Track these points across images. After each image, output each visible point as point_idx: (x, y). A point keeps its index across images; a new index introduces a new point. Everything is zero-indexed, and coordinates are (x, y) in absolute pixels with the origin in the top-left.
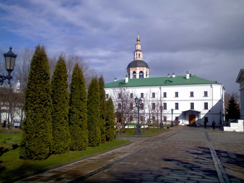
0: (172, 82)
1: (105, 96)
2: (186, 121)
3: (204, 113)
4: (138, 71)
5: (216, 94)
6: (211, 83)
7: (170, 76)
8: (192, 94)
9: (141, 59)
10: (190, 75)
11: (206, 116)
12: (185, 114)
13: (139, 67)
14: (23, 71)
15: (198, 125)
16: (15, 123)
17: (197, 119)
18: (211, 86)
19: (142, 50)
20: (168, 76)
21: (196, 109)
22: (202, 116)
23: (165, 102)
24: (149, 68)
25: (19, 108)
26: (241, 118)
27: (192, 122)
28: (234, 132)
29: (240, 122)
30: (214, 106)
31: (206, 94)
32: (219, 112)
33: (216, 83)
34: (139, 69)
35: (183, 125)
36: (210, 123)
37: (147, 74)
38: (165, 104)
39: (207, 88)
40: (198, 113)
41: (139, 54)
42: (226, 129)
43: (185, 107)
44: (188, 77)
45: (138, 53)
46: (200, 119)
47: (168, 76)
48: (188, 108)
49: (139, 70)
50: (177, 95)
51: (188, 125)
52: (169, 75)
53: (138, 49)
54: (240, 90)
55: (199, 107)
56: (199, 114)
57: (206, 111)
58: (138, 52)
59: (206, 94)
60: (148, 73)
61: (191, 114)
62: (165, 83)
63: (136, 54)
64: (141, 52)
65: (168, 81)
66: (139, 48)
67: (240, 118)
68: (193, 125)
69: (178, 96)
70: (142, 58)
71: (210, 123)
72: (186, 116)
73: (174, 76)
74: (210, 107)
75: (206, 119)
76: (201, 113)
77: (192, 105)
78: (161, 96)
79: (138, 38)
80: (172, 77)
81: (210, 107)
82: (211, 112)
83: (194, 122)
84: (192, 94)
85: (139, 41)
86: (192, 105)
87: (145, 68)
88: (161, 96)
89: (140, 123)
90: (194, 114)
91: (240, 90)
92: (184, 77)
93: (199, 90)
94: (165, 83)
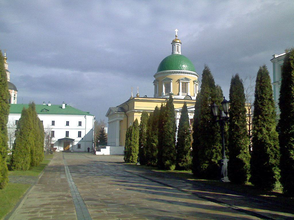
0: (48, 111)
2: (61, 148)
3: (77, 140)
5: (88, 124)
6: (85, 114)
7: (45, 104)
8: (68, 123)
10: (66, 105)
11: (79, 144)
12: (60, 141)
15: (72, 151)
17: (71, 146)
18: (85, 117)
19: (8, 70)
20: (44, 104)
21: (71, 136)
22: (76, 143)
23: (53, 130)
24: (17, 91)
25: (129, 127)
26: (108, 145)
27: (66, 149)
28: (103, 155)
29: (108, 148)
30: (86, 134)
31: (80, 124)
32: (91, 140)
33: (88, 114)
35: (59, 151)
36: (83, 148)
37: (15, 97)
38: (53, 132)
39: (81, 118)
40: (73, 140)
42: (97, 153)
43: (59, 135)
44: (64, 107)
46: (74, 145)
47: (44, 104)
48: (63, 136)
50: (53, 124)
51: (63, 151)
52: (45, 103)
54: (108, 123)
55: (73, 135)
56: (73, 142)
57: (80, 139)
59: (80, 124)
60: (16, 96)
61: (66, 142)
62: (42, 111)
65: (45, 110)
67: (281, 96)
68: (67, 151)
69: (54, 125)
70: (9, 80)
71: (83, 148)
72: (61, 143)
73: (50, 105)
74: (83, 135)
75: (79, 146)
76: (75, 140)
77: (67, 133)
79: (5, 56)
80: (48, 105)
81: (83, 135)
82: (84, 140)
83: (68, 148)
84: (68, 123)
85: (6, 60)
86: (67, 133)
87: (13, 91)
90: (68, 141)
91: (108, 123)
92: (59, 106)
93: (74, 120)
94: (42, 111)
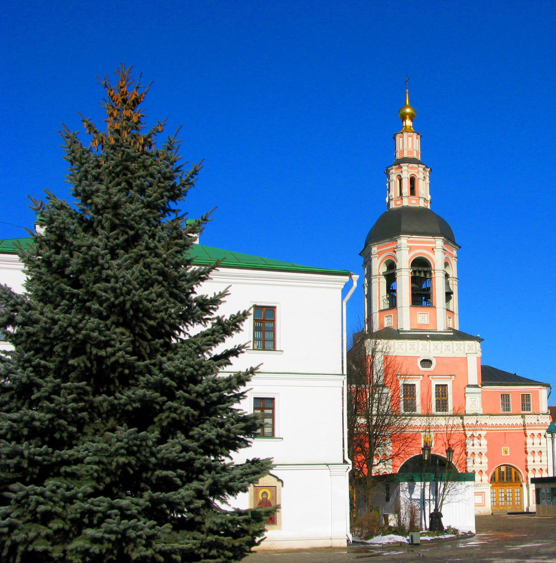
1: (257, 414)
4: (406, 176)
9: (422, 204)
13: (406, 233)
14: (521, 486)
16: (467, 413)
34: (411, 249)
37: (447, 276)
41: (412, 181)
45: (406, 171)
49: (410, 251)
53: (406, 155)
58: (405, 166)
63: (378, 267)
64: (421, 169)
66: (410, 152)
78: (553, 442)
87: (439, 242)
88: (553, 442)
89: (354, 386)
